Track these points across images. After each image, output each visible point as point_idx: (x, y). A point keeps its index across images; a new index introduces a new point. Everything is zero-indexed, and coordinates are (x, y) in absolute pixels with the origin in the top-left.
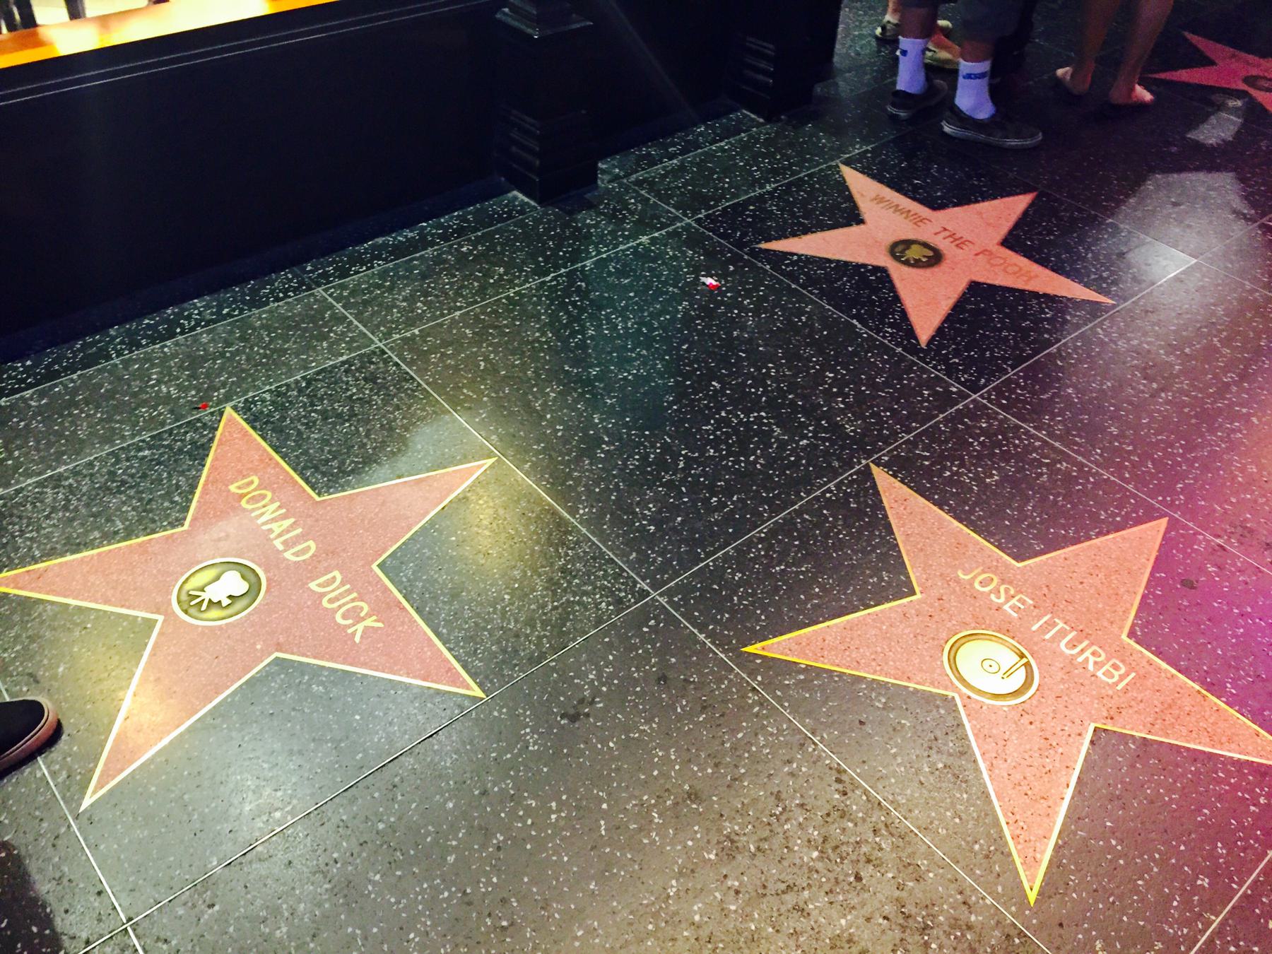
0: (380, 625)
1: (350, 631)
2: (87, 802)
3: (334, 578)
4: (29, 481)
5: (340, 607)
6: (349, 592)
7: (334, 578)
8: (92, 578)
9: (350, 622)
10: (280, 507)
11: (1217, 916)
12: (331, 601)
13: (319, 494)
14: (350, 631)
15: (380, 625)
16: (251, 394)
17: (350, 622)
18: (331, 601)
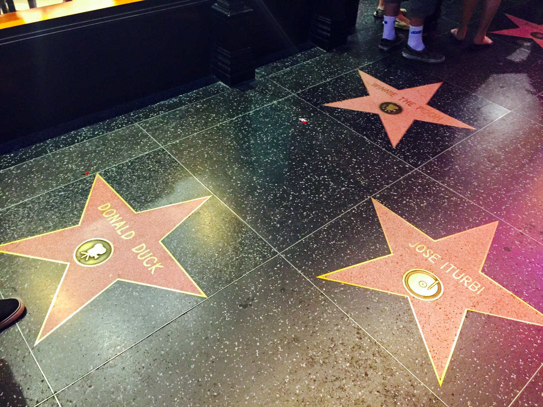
0: (162, 267)
1: (149, 269)
2: (37, 342)
3: (143, 247)
4: (13, 205)
5: (145, 259)
6: (149, 253)
7: (143, 247)
8: (39, 247)
9: (149, 265)
10: (119, 216)
11: (520, 391)
12: (141, 256)
13: (136, 211)
14: (149, 269)
15: (162, 267)
16: (107, 168)
17: (149, 265)
18: (141, 256)
